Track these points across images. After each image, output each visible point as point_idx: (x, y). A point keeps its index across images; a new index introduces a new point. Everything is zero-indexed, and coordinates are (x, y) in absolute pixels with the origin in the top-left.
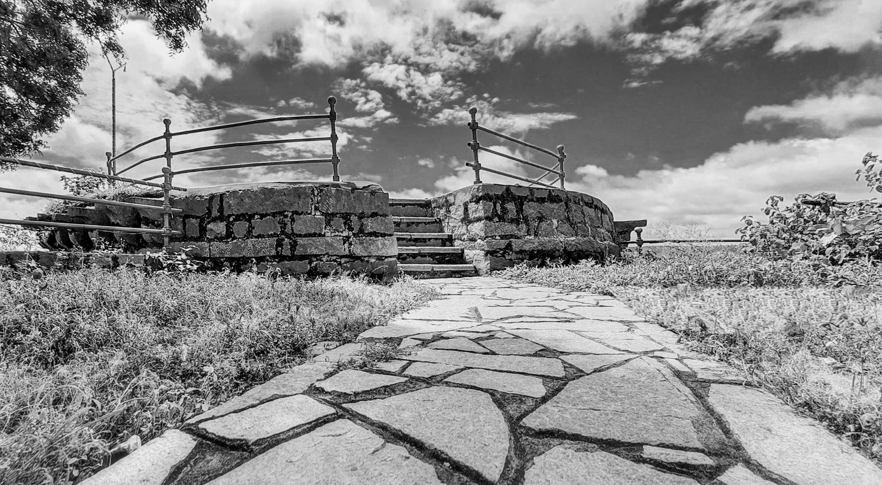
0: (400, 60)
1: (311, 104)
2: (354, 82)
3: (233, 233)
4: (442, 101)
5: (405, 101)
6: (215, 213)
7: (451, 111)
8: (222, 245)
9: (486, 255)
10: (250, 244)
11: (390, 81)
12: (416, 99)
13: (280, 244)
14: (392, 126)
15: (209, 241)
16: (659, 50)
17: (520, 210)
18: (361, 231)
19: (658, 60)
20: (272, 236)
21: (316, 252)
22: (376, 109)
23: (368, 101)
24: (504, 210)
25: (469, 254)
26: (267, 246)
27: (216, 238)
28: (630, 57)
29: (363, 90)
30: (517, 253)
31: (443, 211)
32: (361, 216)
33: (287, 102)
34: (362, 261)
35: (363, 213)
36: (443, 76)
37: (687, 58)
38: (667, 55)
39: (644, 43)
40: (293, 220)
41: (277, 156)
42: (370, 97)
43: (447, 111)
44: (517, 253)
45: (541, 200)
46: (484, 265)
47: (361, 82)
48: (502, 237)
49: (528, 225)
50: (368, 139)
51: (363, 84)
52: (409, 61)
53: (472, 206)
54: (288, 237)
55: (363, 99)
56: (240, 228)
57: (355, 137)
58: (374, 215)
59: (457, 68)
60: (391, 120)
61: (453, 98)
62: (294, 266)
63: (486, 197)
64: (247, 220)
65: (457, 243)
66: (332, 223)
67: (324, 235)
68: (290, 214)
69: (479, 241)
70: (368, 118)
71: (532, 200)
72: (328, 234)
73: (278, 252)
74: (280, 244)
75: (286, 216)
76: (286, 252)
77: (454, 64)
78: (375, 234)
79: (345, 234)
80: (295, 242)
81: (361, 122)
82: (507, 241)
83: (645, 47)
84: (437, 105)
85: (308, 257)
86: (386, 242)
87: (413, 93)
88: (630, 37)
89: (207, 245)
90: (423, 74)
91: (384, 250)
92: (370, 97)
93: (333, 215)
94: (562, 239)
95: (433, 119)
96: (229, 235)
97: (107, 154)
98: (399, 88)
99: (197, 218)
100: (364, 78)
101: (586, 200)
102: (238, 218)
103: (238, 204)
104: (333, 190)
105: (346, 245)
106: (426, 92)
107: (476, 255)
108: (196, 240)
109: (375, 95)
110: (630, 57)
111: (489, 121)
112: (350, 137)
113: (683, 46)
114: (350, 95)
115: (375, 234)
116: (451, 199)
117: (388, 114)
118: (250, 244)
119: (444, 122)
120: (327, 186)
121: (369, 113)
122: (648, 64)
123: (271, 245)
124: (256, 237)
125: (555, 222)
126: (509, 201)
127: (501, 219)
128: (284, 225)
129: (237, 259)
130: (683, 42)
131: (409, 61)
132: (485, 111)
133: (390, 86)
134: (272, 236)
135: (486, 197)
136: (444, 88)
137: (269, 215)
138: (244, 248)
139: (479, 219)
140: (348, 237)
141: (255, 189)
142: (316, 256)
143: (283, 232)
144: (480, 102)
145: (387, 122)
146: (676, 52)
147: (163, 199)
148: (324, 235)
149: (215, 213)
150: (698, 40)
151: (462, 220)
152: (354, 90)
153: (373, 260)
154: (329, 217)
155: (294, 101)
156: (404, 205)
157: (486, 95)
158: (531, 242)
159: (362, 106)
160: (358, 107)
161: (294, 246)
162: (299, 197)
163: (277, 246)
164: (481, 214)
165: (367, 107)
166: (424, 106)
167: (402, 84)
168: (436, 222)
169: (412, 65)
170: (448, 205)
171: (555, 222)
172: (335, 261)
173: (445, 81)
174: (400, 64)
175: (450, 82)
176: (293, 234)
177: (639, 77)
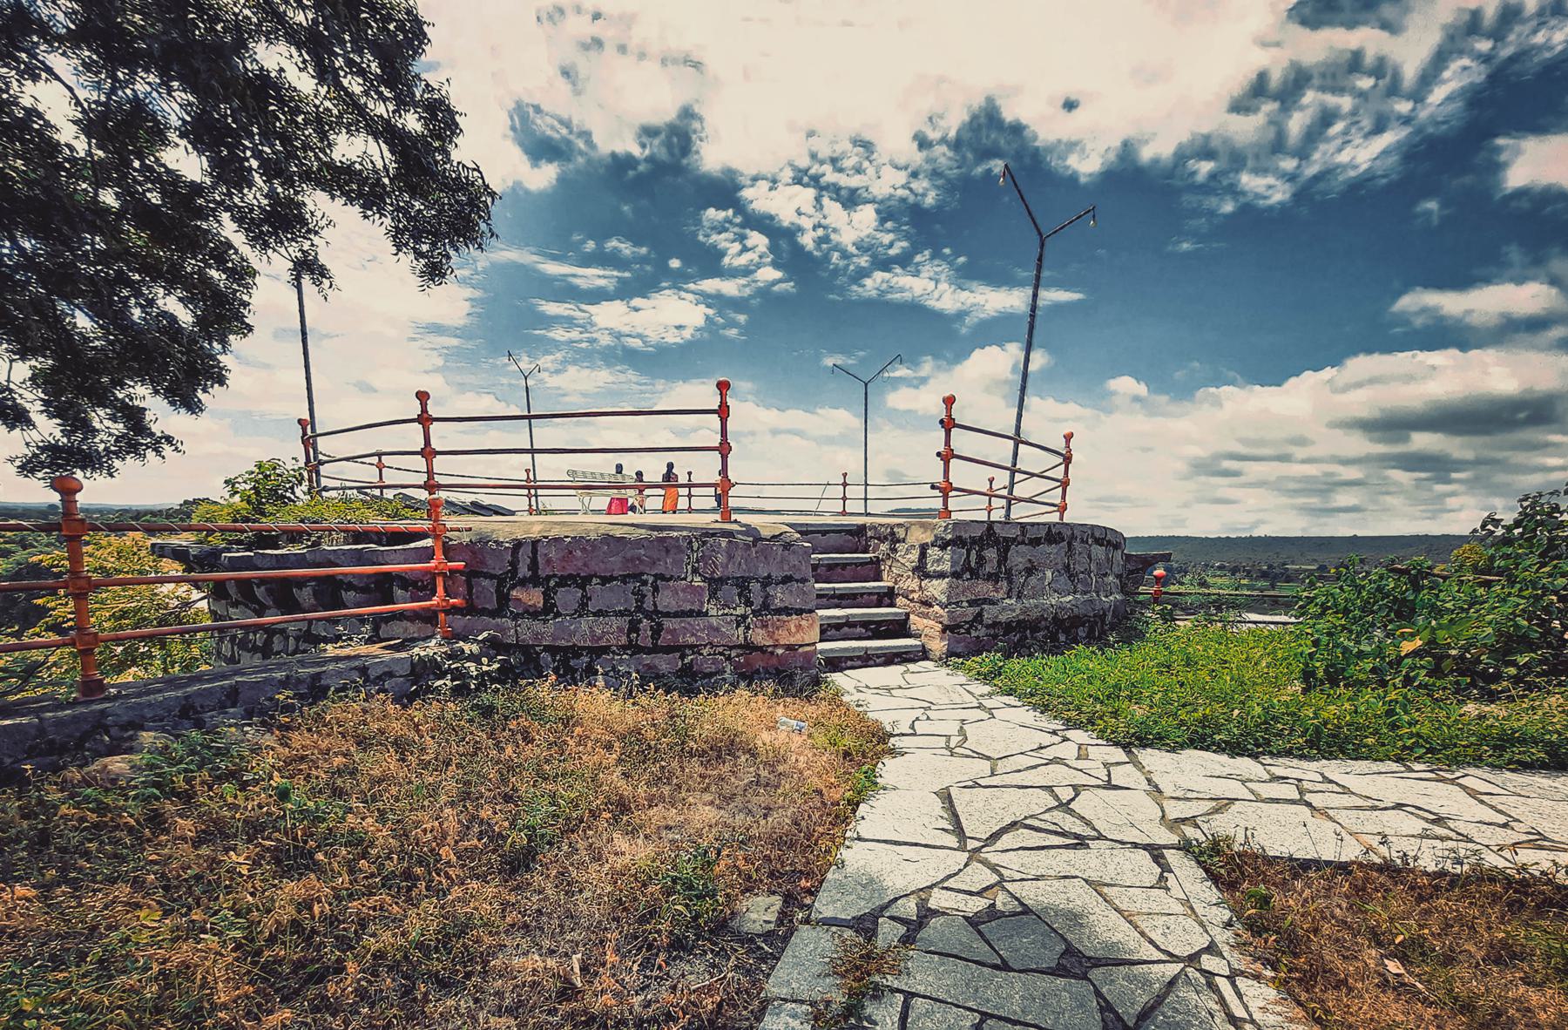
0: (806, 179)
1: (644, 250)
2: (722, 215)
3: (555, 605)
4: (874, 257)
5: (810, 253)
6: (524, 571)
7: (887, 275)
8: (538, 626)
9: (944, 631)
10: (584, 626)
11: (786, 217)
12: (830, 249)
13: (634, 627)
14: (782, 299)
15: (515, 617)
16: (1234, 191)
17: (1003, 559)
18: (765, 606)
19: (1228, 207)
20: (621, 614)
21: (691, 640)
22: (759, 266)
23: (745, 249)
24: (981, 558)
25: (916, 622)
26: (612, 630)
27: (527, 611)
28: (1189, 200)
29: (736, 230)
30: (988, 627)
31: (884, 547)
32: (767, 582)
33: (600, 245)
34: (764, 652)
35: (769, 576)
36: (878, 212)
37: (1271, 208)
38: (1242, 200)
39: (1213, 176)
40: (656, 589)
41: (581, 341)
42: (749, 243)
43: (879, 276)
44: (988, 627)
45: (1035, 542)
46: (938, 646)
47: (735, 215)
48: (971, 603)
49: (1010, 582)
50: (742, 318)
51: (738, 220)
52: (823, 181)
53: (934, 553)
54: (648, 615)
55: (737, 247)
56: (567, 598)
57: (720, 314)
58: (787, 580)
59: (903, 200)
60: (783, 285)
61: (892, 252)
62: (657, 662)
63: (958, 542)
64: (578, 586)
65: (900, 601)
66: (719, 594)
67: (706, 614)
68: (651, 579)
69: (937, 608)
70: (743, 281)
71: (1023, 543)
72: (713, 612)
73: (630, 641)
74: (634, 627)
75: (645, 583)
76: (645, 638)
77: (900, 192)
78: (787, 611)
79: (740, 611)
80: (660, 625)
81: (730, 287)
82: (978, 609)
83: (1212, 184)
84: (863, 264)
85: (681, 649)
86: (804, 623)
87: (825, 239)
88: (1192, 164)
89: (511, 623)
90: (845, 206)
91: (798, 636)
92: (749, 243)
93: (722, 581)
94: (1057, 599)
95: (855, 288)
96: (549, 609)
97: (300, 421)
98: (800, 229)
99: (492, 577)
100: (739, 206)
101: (1097, 535)
102: (563, 581)
103: (563, 559)
104: (724, 542)
105: (741, 629)
106: (847, 238)
107: (928, 629)
108: (494, 614)
109: (758, 240)
110: (1189, 200)
111: (947, 296)
112: (710, 312)
113: (1270, 187)
114: (714, 237)
115: (787, 611)
116: (901, 533)
117: (778, 275)
118: (584, 626)
119: (874, 293)
120: (713, 535)
121: (746, 272)
122: (1212, 213)
123: (620, 629)
124: (595, 614)
125: (1049, 574)
126: (989, 546)
127: (975, 574)
128: (641, 597)
129: (565, 649)
130: (1271, 180)
131: (823, 181)
132: (943, 277)
133: (786, 224)
134: (621, 614)
135: (958, 542)
136: (879, 235)
137: (616, 579)
138: (575, 632)
139: (941, 575)
140: (745, 617)
141: (593, 536)
142: (692, 647)
143: (639, 609)
144: (936, 262)
145: (776, 288)
146: (1258, 196)
147: (428, 542)
148: (706, 614)
149: (524, 571)
150: (1291, 178)
151: (914, 570)
152: (721, 228)
153: (780, 651)
154: (715, 584)
155: (613, 243)
156: (824, 533)
157: (947, 251)
158: (1009, 608)
159: (734, 257)
160: (726, 260)
161: (657, 631)
162: (668, 551)
163: (630, 631)
164: (946, 567)
165: (743, 260)
166: (842, 263)
167: (806, 223)
168: (871, 562)
169: (826, 188)
170: (893, 539)
171: (1049, 574)
172: (721, 654)
173: (883, 221)
174: (806, 186)
175: (889, 225)
176: (656, 612)
177: (1196, 235)
